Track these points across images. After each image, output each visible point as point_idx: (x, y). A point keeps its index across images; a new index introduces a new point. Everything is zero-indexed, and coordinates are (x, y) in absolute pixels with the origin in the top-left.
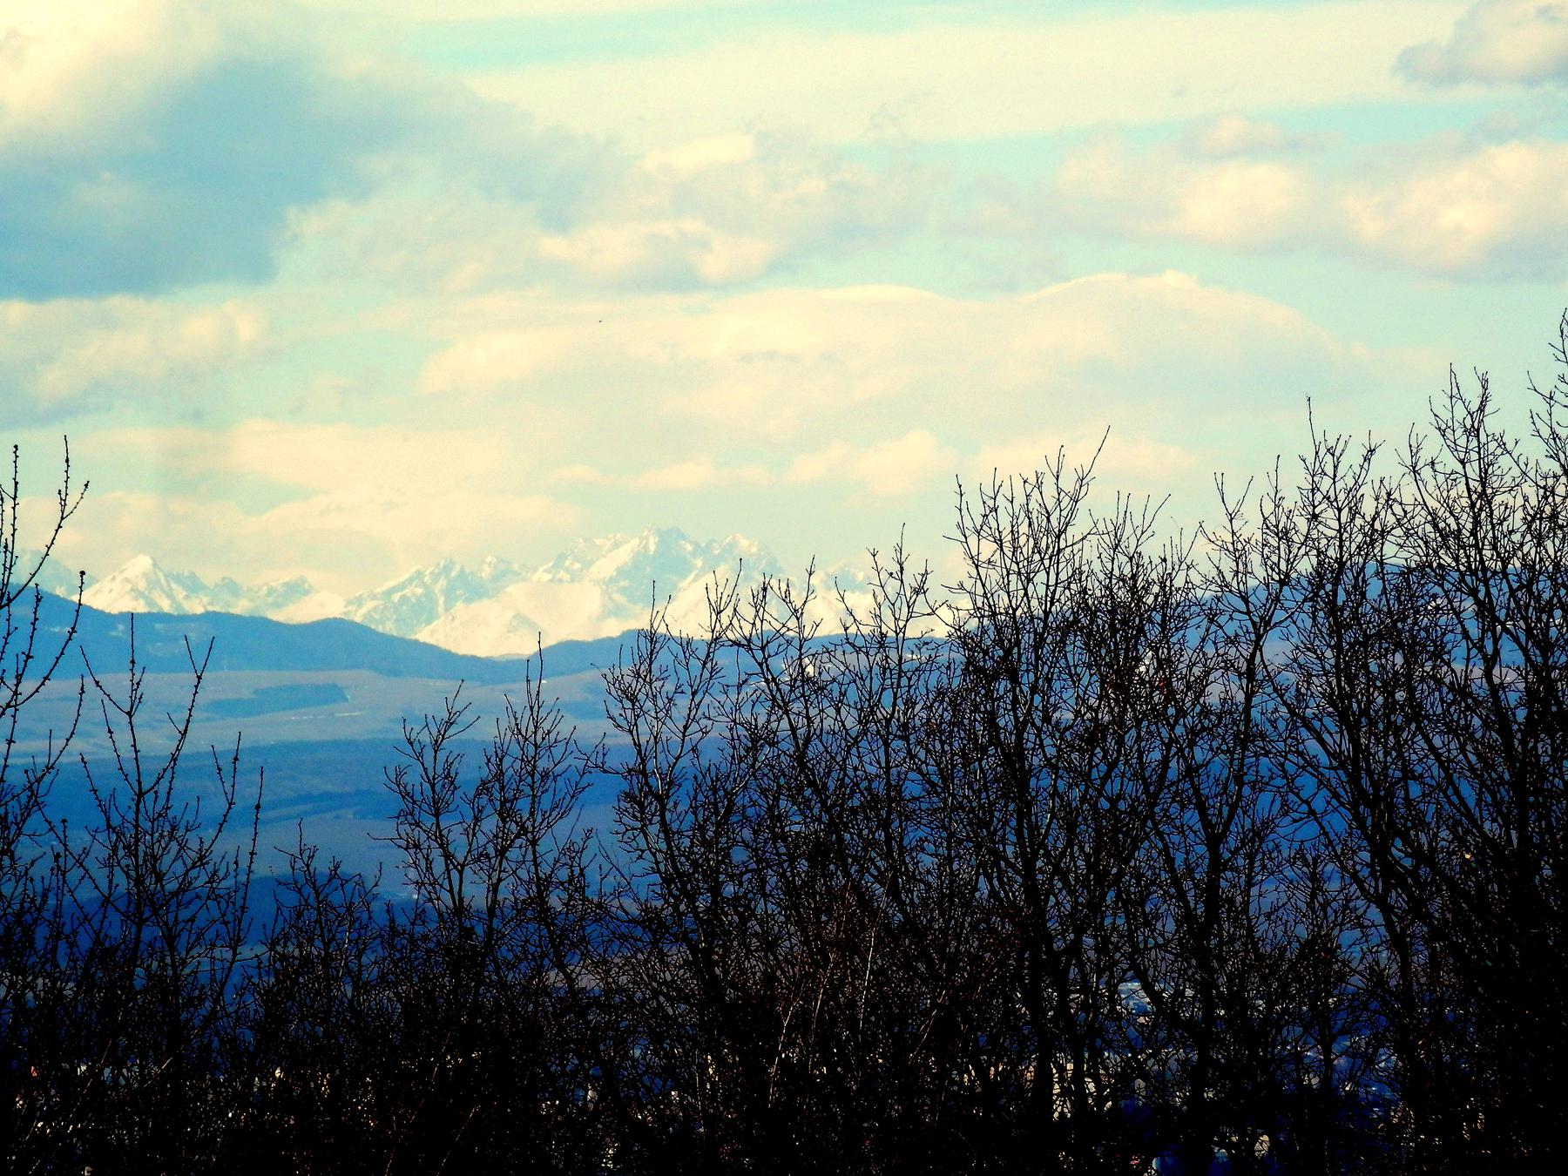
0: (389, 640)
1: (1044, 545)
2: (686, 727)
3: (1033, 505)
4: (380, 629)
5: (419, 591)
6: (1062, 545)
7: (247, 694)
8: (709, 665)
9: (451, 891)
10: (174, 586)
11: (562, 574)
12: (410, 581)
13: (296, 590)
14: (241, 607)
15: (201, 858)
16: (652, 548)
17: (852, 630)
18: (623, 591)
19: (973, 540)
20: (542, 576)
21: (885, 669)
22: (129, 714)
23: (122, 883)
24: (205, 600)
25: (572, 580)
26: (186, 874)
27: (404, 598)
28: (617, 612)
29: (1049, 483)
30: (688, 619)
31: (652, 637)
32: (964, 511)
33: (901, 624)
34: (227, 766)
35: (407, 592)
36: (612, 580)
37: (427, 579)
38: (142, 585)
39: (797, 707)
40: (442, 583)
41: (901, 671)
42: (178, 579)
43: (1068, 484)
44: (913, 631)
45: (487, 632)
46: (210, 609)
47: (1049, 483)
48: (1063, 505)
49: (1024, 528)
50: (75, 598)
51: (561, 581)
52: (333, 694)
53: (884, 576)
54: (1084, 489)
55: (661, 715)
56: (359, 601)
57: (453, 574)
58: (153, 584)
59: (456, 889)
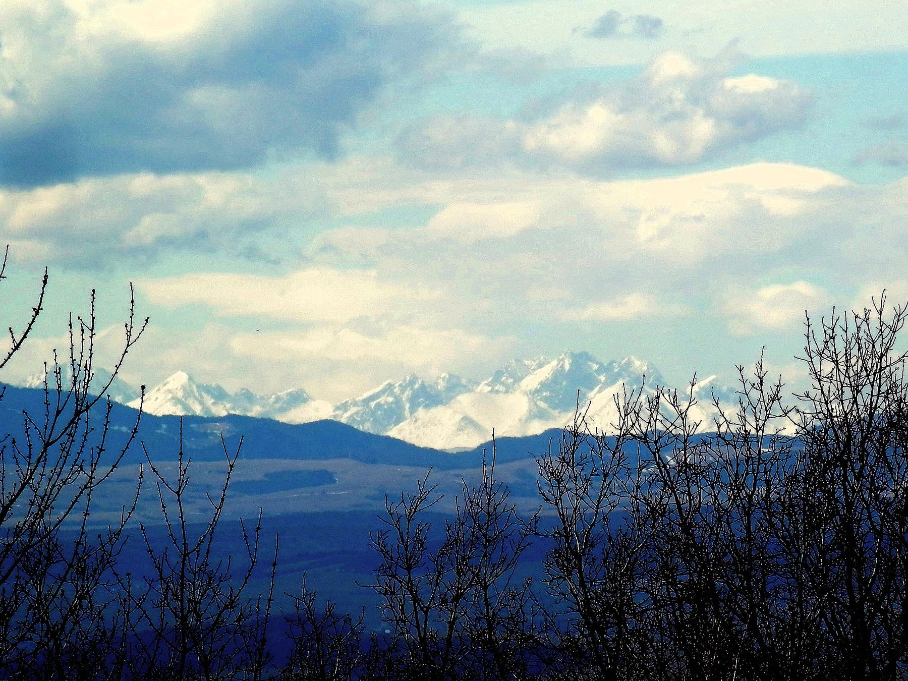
0: (367, 436)
1: (870, 365)
2: (599, 502)
3: (862, 334)
4: (361, 428)
5: (391, 399)
6: (884, 365)
7: (258, 477)
8: (617, 455)
9: (418, 627)
10: (205, 395)
11: (498, 387)
12: (383, 392)
13: (298, 398)
14: (255, 411)
15: (232, 602)
16: (567, 367)
17: (723, 429)
18: (545, 399)
19: (816, 360)
20: (484, 388)
21: (749, 458)
22: (178, 493)
23: (173, 622)
24: (228, 406)
25: (507, 392)
26: (219, 615)
27: (379, 406)
28: (541, 415)
29: (874, 316)
30: (602, 417)
31: (575, 434)
32: (811, 338)
33: (761, 423)
34: (252, 531)
35: (382, 400)
36: (537, 391)
37: (397, 390)
38: (180, 394)
39: (681, 488)
40: (408, 393)
41: (760, 458)
42: (208, 390)
43: (889, 316)
44: (770, 430)
45: (440, 430)
46: (232, 412)
47: (874, 316)
48: (884, 334)
49: (855, 352)
50: (135, 404)
51: (497, 392)
52: (325, 477)
53: (748, 386)
54: (900, 323)
55: (580, 492)
56: (344, 407)
57: (416, 386)
58: (188, 393)
59: (422, 625)
